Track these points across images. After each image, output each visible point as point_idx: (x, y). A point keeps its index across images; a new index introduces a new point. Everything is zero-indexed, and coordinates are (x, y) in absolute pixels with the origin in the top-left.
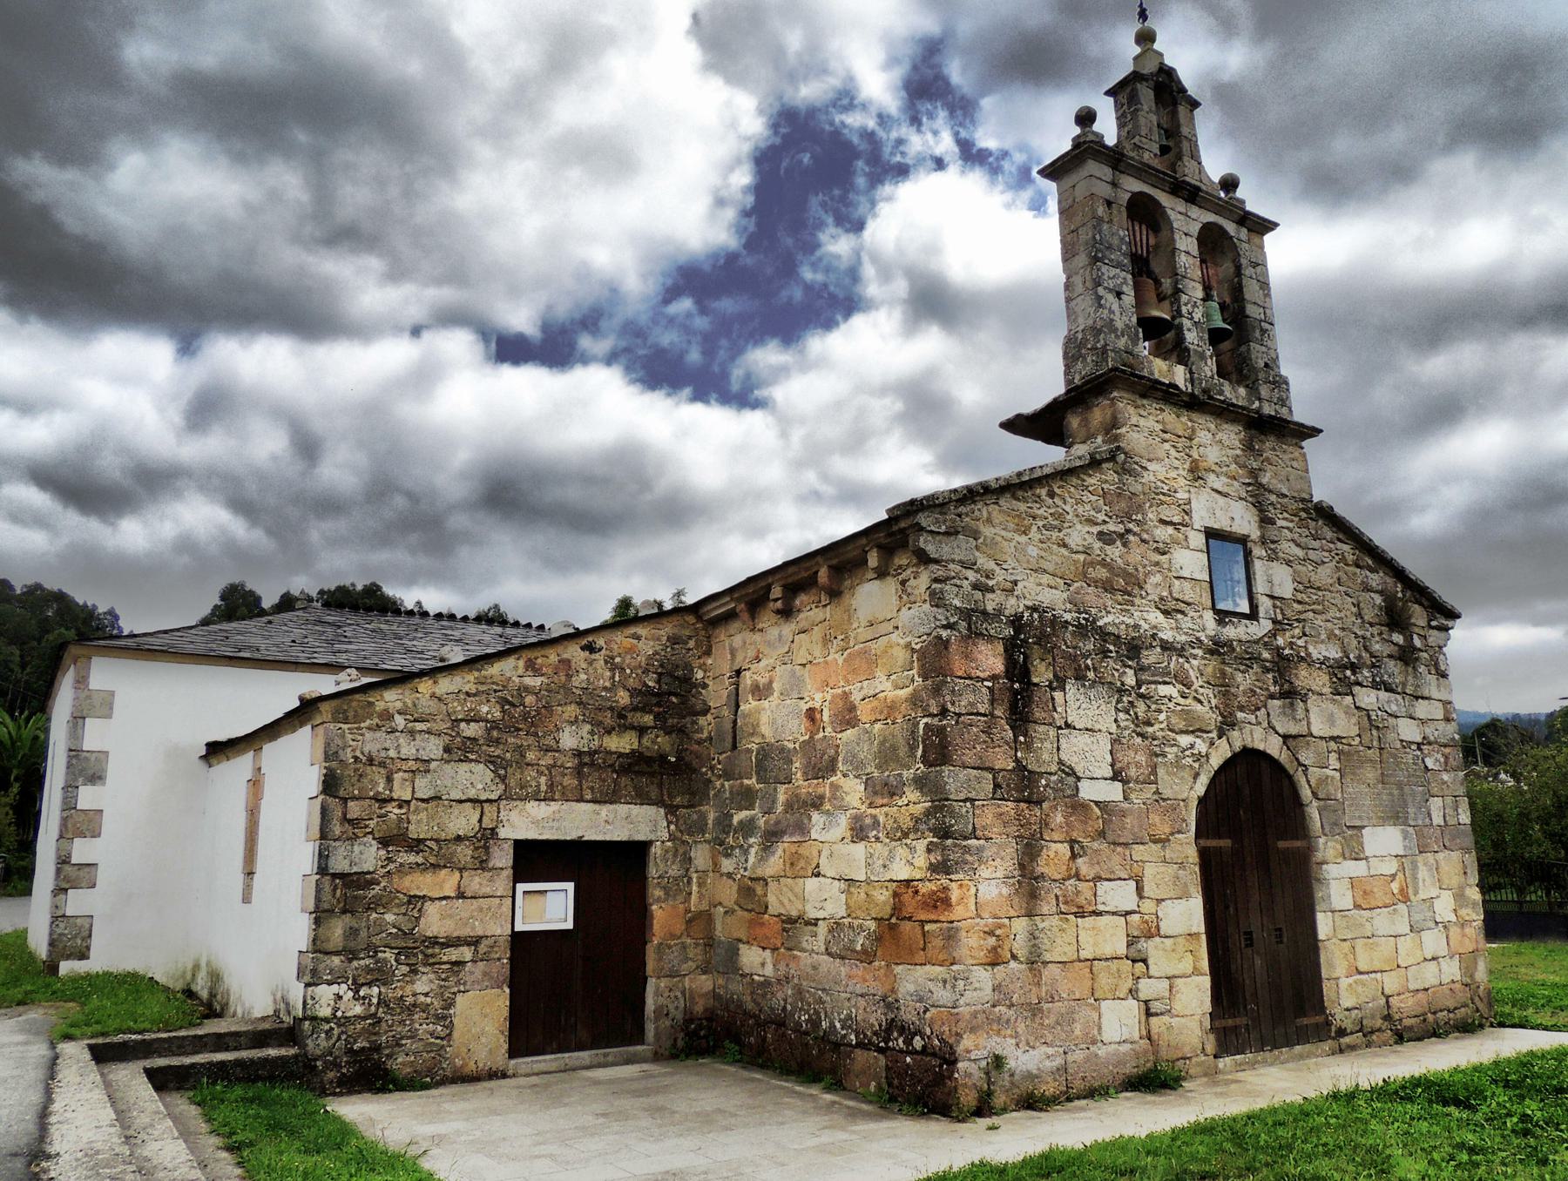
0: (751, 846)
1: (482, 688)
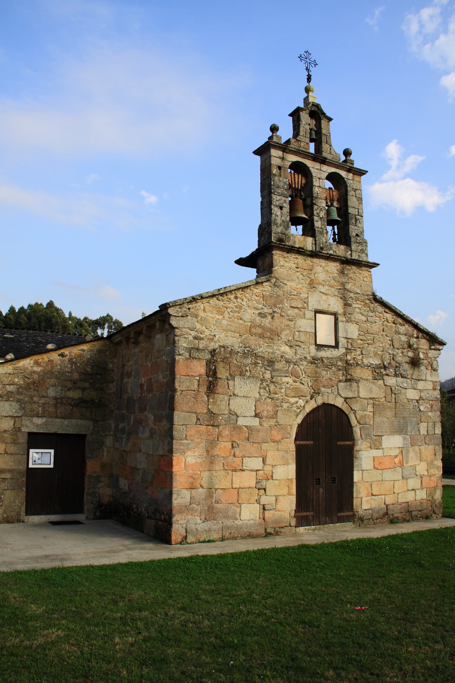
0: (124, 438)
1: (15, 372)
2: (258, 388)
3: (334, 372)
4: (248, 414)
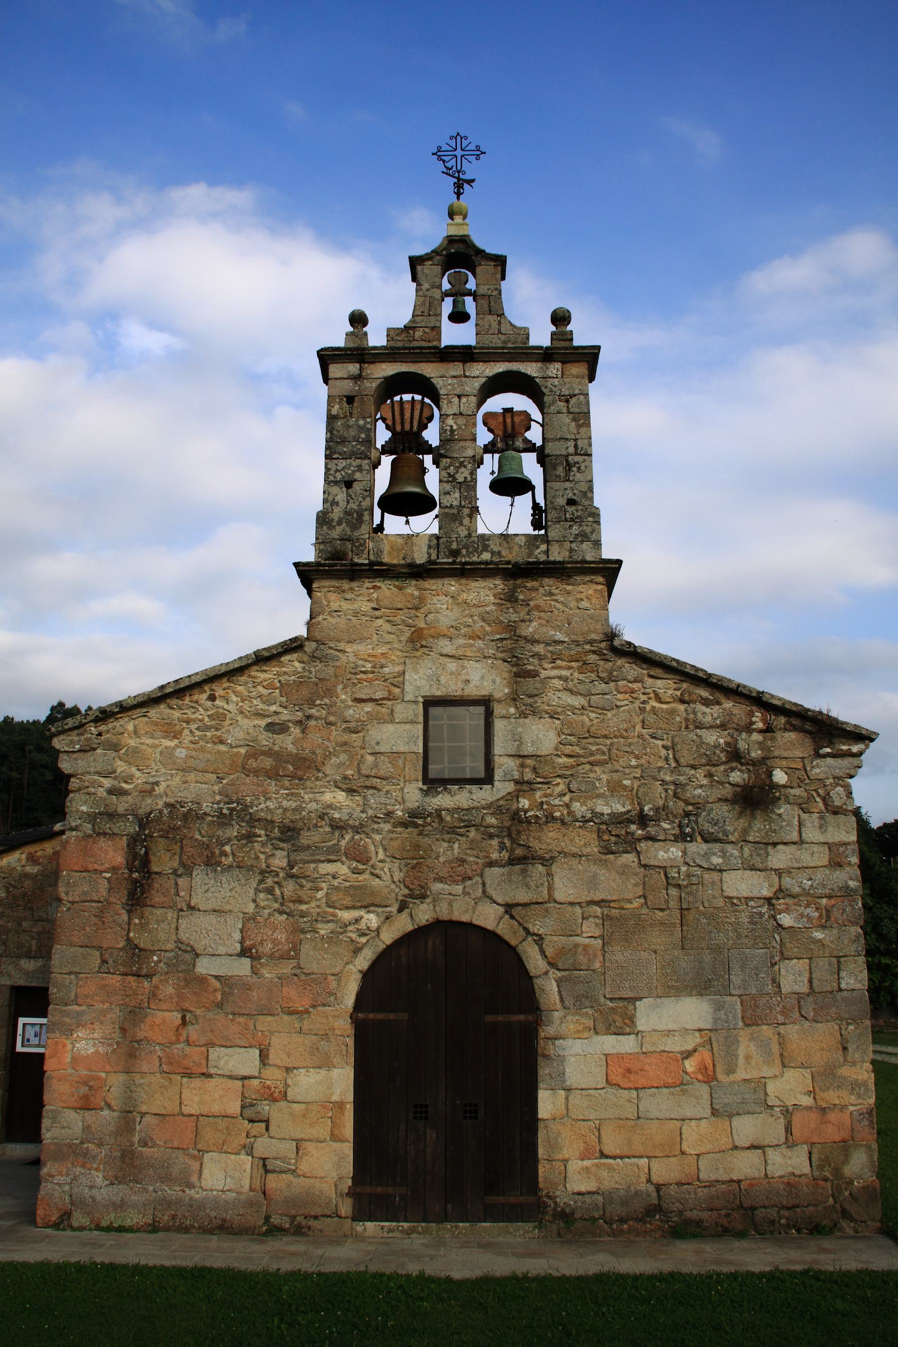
2: (252, 891)
3: (472, 841)
4: (222, 950)
